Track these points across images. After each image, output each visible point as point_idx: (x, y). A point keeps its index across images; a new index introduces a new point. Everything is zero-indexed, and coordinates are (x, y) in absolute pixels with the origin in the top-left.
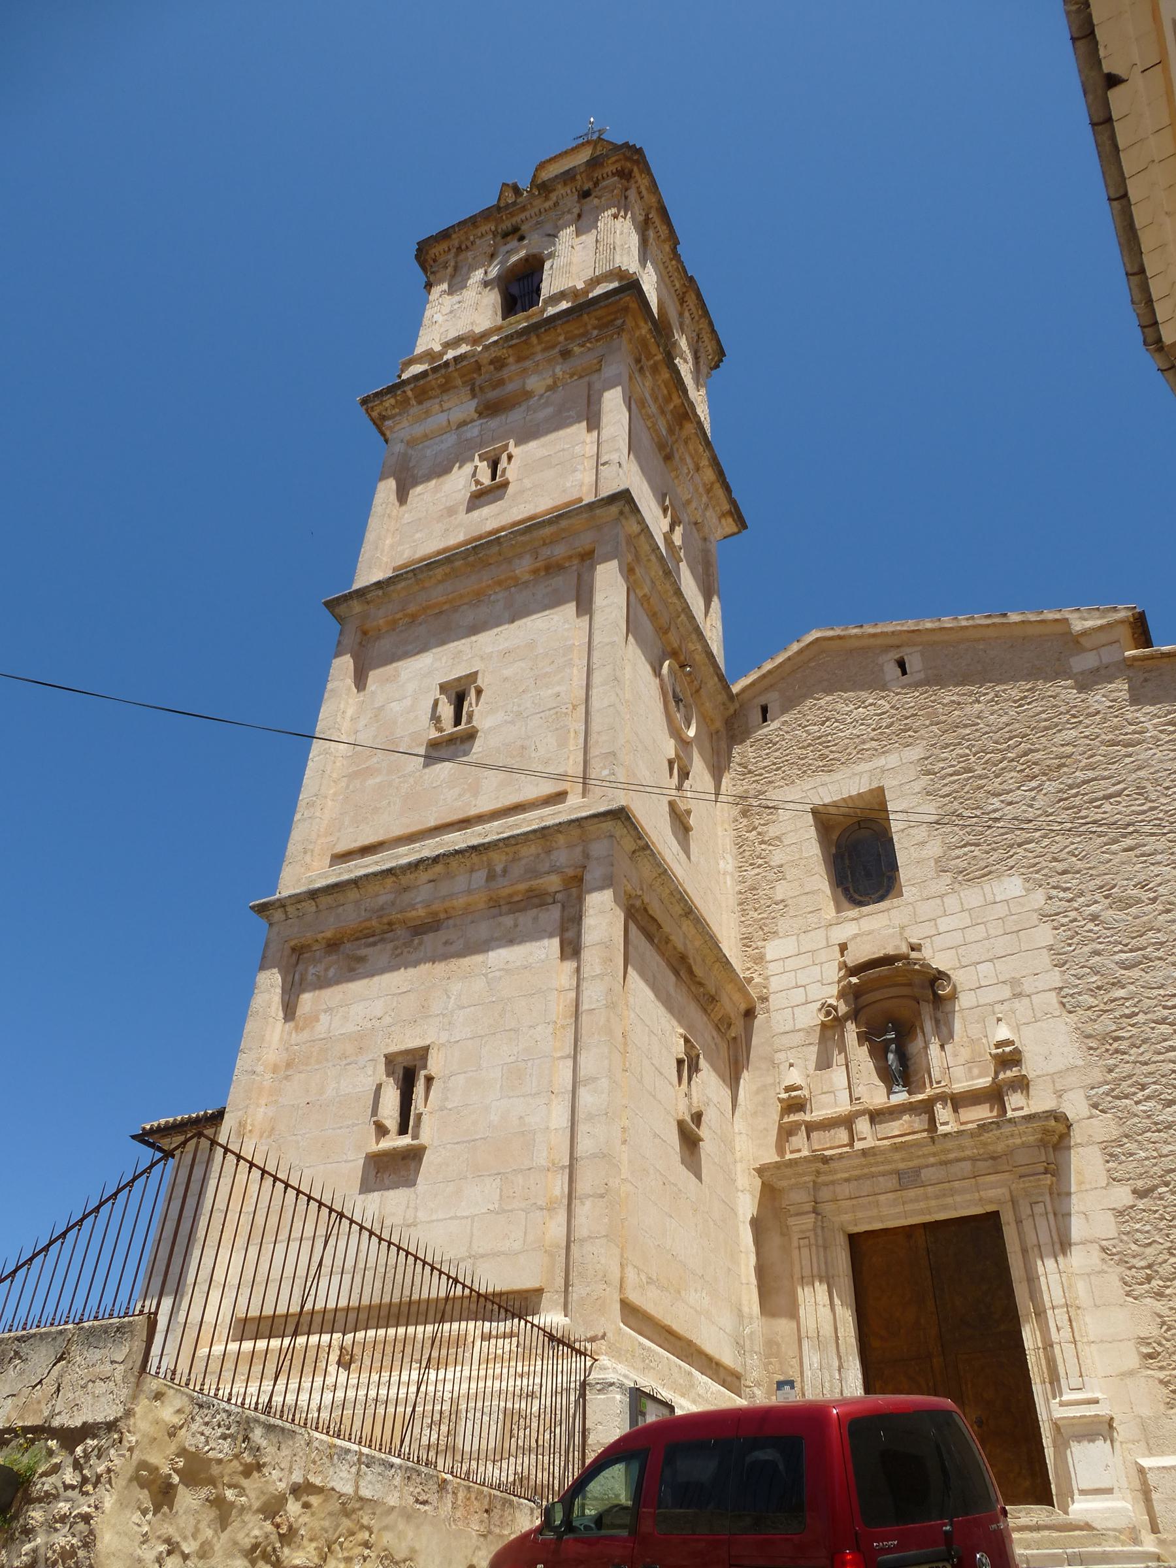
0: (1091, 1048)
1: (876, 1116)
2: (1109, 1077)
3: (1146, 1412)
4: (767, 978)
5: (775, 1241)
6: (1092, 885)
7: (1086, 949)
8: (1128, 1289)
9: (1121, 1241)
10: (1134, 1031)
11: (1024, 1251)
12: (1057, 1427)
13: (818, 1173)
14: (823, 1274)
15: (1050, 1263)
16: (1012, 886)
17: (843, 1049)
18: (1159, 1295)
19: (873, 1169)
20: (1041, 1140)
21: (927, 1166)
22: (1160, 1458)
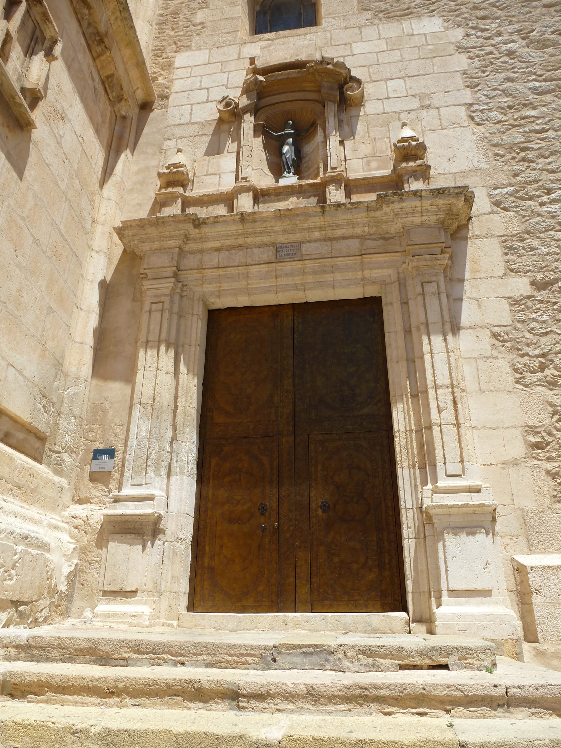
0: (497, 155)
1: (260, 196)
2: (514, 181)
3: (528, 504)
4: (172, 81)
5: (124, 305)
6: (510, 28)
7: (500, 76)
8: (518, 376)
9: (515, 329)
10: (543, 144)
11: (408, 332)
12: (426, 516)
13: (186, 238)
14: (173, 340)
15: (437, 341)
16: (431, 25)
17: (237, 137)
18: (552, 384)
19: (249, 240)
20: (443, 222)
21: (309, 242)
22: (542, 556)
